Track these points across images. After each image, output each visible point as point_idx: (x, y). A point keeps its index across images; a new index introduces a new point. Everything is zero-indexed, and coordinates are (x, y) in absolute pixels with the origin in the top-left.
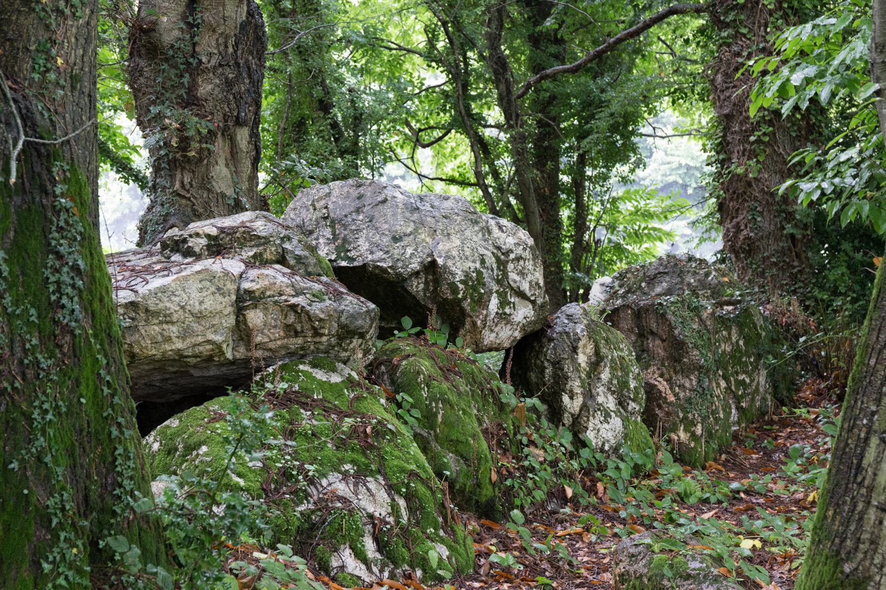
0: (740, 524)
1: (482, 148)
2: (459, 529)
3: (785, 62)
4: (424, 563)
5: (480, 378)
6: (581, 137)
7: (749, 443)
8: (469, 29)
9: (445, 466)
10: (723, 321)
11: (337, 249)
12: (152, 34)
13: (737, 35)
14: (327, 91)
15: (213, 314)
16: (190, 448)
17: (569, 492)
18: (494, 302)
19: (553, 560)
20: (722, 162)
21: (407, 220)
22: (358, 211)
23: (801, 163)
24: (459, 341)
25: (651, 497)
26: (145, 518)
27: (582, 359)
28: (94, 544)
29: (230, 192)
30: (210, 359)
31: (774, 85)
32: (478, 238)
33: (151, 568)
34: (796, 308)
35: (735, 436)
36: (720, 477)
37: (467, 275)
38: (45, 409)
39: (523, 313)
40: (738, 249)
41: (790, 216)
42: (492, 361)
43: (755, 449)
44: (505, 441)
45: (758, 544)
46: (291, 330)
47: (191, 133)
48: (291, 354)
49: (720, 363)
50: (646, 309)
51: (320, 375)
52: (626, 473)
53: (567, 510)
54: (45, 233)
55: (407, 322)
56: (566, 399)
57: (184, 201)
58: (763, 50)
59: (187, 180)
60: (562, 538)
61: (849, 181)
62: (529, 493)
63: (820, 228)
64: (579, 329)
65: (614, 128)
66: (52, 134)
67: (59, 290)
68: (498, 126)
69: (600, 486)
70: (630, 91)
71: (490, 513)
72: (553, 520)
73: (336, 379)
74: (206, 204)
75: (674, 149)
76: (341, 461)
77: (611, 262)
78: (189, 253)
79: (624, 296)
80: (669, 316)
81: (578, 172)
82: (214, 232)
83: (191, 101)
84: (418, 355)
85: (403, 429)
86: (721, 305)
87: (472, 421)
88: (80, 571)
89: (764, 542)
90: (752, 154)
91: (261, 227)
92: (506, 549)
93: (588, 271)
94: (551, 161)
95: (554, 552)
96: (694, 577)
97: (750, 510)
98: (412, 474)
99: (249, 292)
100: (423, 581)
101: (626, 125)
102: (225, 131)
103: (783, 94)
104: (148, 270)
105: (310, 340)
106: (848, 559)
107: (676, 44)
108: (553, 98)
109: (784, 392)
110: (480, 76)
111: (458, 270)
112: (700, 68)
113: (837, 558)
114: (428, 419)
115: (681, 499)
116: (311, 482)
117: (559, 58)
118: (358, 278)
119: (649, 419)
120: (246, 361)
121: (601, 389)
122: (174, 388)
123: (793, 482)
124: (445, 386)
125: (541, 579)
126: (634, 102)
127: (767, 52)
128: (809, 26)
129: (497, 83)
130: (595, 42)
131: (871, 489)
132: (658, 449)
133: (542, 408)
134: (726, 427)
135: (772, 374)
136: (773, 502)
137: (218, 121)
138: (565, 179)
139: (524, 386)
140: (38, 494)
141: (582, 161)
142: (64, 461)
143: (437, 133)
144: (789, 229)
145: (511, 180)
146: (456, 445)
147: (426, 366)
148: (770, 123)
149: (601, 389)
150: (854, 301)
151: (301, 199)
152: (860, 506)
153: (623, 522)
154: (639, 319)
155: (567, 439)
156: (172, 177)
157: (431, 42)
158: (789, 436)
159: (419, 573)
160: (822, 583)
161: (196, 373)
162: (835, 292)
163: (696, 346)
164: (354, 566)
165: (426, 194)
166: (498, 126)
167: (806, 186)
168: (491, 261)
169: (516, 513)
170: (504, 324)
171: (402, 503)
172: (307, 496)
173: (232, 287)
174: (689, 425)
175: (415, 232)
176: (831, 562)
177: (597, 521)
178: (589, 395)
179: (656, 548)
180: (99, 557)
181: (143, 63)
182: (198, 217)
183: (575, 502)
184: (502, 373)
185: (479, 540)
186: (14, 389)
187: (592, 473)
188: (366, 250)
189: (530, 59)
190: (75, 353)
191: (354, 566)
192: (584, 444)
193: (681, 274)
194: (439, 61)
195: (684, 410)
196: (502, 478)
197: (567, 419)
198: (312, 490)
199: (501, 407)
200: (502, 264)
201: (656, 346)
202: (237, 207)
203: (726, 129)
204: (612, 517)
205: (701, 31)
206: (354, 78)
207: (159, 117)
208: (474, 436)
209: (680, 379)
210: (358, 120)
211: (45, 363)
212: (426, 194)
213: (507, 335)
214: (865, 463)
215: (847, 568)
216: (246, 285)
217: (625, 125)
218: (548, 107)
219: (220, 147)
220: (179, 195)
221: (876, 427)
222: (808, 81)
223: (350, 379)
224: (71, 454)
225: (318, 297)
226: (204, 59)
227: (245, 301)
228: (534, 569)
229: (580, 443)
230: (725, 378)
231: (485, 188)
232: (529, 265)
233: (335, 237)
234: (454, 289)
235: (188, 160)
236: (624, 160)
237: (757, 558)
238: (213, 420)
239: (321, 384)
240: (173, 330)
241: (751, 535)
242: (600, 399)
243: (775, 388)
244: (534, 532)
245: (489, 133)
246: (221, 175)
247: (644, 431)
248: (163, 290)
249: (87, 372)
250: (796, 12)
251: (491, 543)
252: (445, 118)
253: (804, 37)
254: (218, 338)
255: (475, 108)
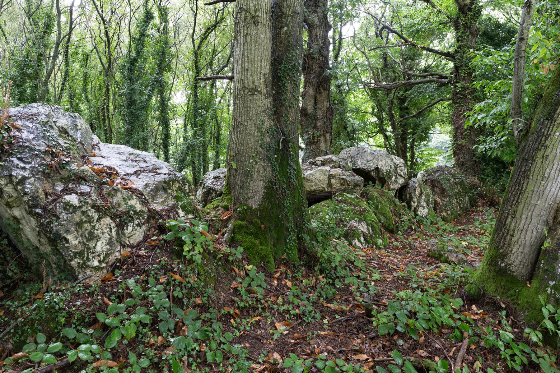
0: (461, 238)
1: (386, 138)
2: (385, 236)
3: (475, 113)
4: (376, 244)
5: (390, 197)
6: (413, 134)
7: (463, 216)
8: (383, 107)
9: (381, 220)
10: (456, 184)
11: (353, 164)
13: (460, 106)
14: (346, 124)
15: (323, 180)
16: (317, 213)
17: (413, 228)
18: (394, 178)
19: (410, 245)
20: (455, 141)
21: (371, 157)
22: (358, 154)
23: (479, 140)
24: (384, 188)
25: (436, 230)
26: (310, 229)
27: (417, 193)
28: (298, 235)
29: (324, 150)
30: (322, 191)
31: (472, 120)
32: (389, 161)
33: (313, 242)
34: (476, 180)
35: (459, 214)
36: (455, 225)
37: (387, 171)
38: (287, 202)
39: (401, 181)
40: (459, 164)
41: (475, 155)
42: (392, 193)
43: (465, 218)
44: (397, 214)
45: (467, 244)
46: (342, 184)
47: (315, 135)
48: (342, 190)
49: (455, 195)
50: (435, 180)
51: (349, 196)
52: (429, 223)
53: (413, 232)
54: (287, 160)
55: (370, 183)
56: (412, 203)
58: (468, 110)
60: (412, 239)
61: (494, 145)
62: (403, 227)
63: (484, 158)
64: (416, 185)
65: (422, 132)
66: (288, 136)
67: (290, 174)
68: (390, 132)
69: (422, 226)
70: (427, 122)
71: (393, 232)
72: (409, 235)
73: (353, 197)
74: (319, 153)
75: (441, 137)
76: (355, 217)
77: (421, 167)
78: (316, 165)
79: (427, 177)
80: (441, 182)
81: (412, 144)
82: (323, 160)
83: (315, 127)
84: (374, 191)
85: (370, 210)
86: (455, 179)
87: (388, 209)
88: (295, 242)
89: (469, 243)
90: (464, 138)
91: (334, 158)
92: (397, 241)
93: (415, 170)
94: (405, 141)
95: (410, 243)
96: (450, 251)
97: (464, 234)
98: (373, 221)
99: (332, 175)
100: (376, 248)
101: (426, 131)
102: (323, 134)
103: (475, 122)
104: (307, 169)
105: (346, 187)
106: (501, 249)
107: (442, 108)
108: (406, 124)
109: (473, 203)
110: (386, 119)
111: (384, 169)
112: (447, 115)
113: (498, 248)
114: (376, 207)
115: (444, 230)
116: (347, 222)
117: (408, 113)
118: (358, 171)
119: (435, 209)
120: (331, 192)
121: (422, 201)
122: (315, 198)
123: (477, 227)
124: (381, 199)
125: (407, 250)
126: (429, 125)
127: (470, 110)
128: (483, 103)
129: (391, 121)
130: (418, 109)
131: (508, 230)
132: (437, 217)
133: (406, 205)
134: (456, 212)
135: (470, 199)
136: (471, 233)
137: (322, 132)
138: (408, 145)
139: (401, 200)
140: (286, 223)
141: (414, 141)
142: (292, 215)
143: (374, 134)
144: (474, 159)
145: (394, 146)
146: (384, 214)
147: (376, 194)
148: (469, 130)
149: (422, 201)
150: (493, 178)
151: (343, 152)
152: (505, 235)
153: (428, 236)
154: (433, 182)
155: (413, 214)
156: (310, 146)
157: (373, 111)
158: (475, 215)
159: (375, 246)
160: (493, 255)
161: (318, 195)
162: (488, 176)
163: (449, 190)
164: (358, 244)
165: (372, 149)
166: (390, 132)
167: (481, 147)
168: (393, 167)
169: (400, 232)
170: (396, 184)
171: (370, 228)
172: (346, 226)
173: (327, 173)
174: (446, 211)
175: (373, 160)
176: (496, 250)
177: (421, 235)
178: (419, 202)
179: (439, 243)
180: (299, 239)
181: (303, 118)
182: (317, 156)
183: (415, 230)
184: (395, 196)
185: (390, 239)
186: (72, 191)
187: (420, 223)
188: (360, 164)
189: (400, 114)
190: (294, 190)
191: (358, 244)
192: (417, 215)
193: (443, 171)
194: (375, 115)
195: (445, 207)
196: (396, 223)
197: (413, 209)
198: (347, 224)
199: (395, 205)
200: (396, 168)
201: (437, 190)
202: (326, 154)
203: (456, 132)
204: (426, 234)
205: (449, 105)
206: (352, 119)
207: (308, 131)
208: (388, 212)
209: (444, 199)
210: (354, 131)
211: (287, 192)
212: (372, 149)
213: (396, 186)
214: (507, 223)
215: (501, 251)
216: (331, 173)
217: (426, 131)
218: (404, 126)
219: (322, 139)
221: (510, 213)
222: (483, 118)
223: (356, 197)
224: (293, 214)
225: (349, 176)
227: (330, 177)
228: (405, 247)
229: (416, 215)
230: (456, 199)
231: (387, 148)
232: (403, 168)
233: (352, 161)
234: (383, 174)
235: (314, 142)
236: (425, 140)
237: (468, 247)
238: (323, 206)
239: (349, 198)
240: (313, 184)
241: (465, 241)
242: (422, 204)
243: (470, 202)
244: (404, 237)
245: (388, 134)
246: (323, 146)
247: (434, 212)
248: (311, 174)
249: (297, 194)
250: (478, 99)
251: (393, 240)
252: (377, 130)
253: (482, 106)
254: (324, 186)
255: (384, 127)
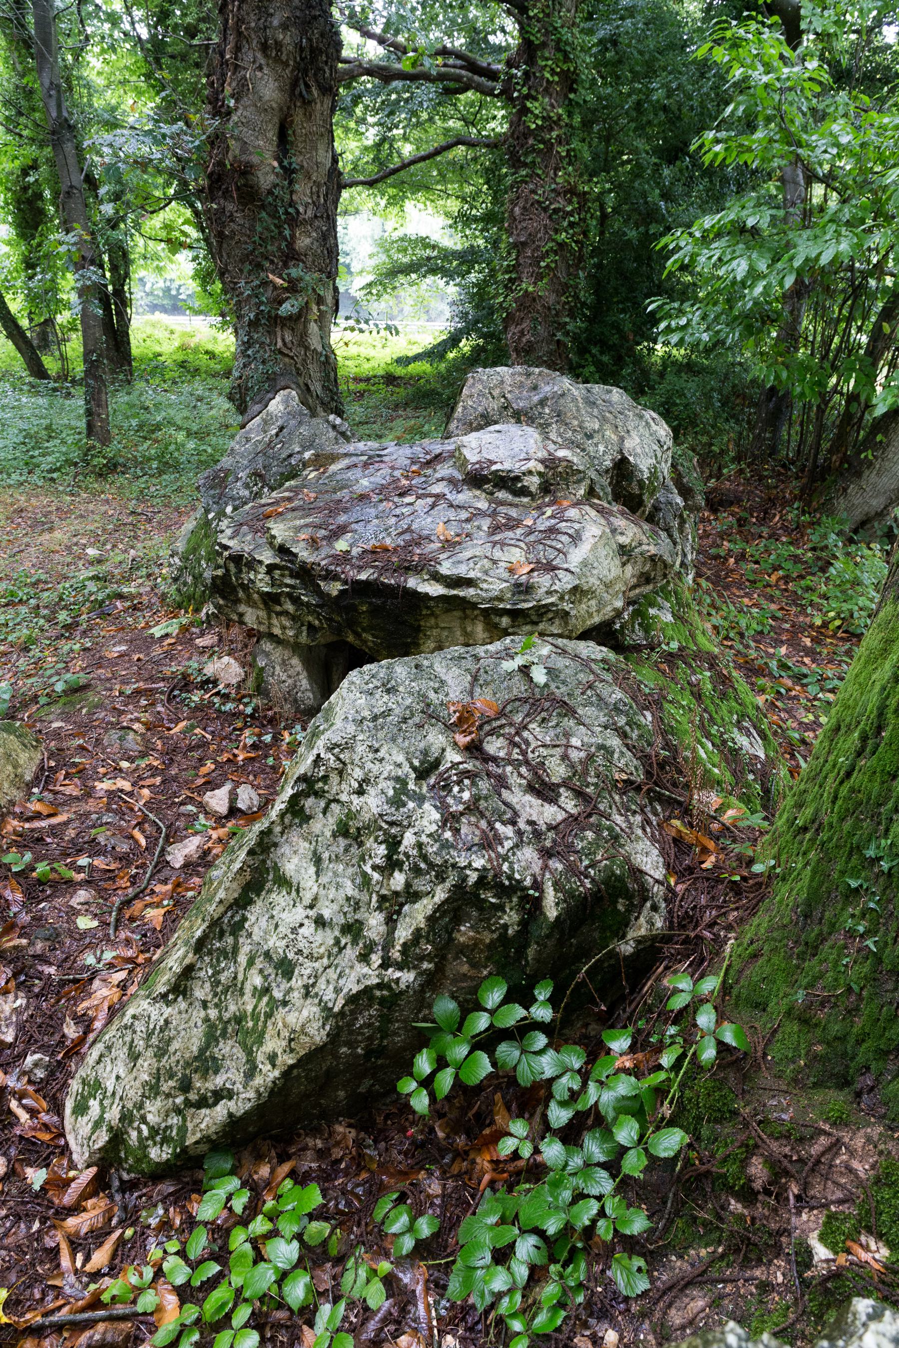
12: (250, 177)
57: (287, 360)
59: (288, 338)
144: (559, 336)
220: (281, 352)
226: (301, 210)
